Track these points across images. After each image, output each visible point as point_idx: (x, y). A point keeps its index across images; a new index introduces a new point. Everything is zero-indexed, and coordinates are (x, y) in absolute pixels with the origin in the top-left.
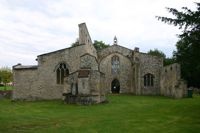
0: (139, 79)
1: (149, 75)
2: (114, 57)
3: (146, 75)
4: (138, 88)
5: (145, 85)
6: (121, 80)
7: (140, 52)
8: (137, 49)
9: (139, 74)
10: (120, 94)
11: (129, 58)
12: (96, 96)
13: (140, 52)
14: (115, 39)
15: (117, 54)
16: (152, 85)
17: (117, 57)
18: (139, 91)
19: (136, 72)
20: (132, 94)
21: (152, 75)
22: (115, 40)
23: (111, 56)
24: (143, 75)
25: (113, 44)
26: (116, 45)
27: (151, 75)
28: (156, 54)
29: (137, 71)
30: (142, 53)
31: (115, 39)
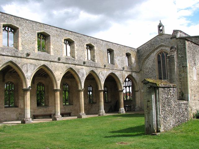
15: (163, 48)
23: (156, 52)
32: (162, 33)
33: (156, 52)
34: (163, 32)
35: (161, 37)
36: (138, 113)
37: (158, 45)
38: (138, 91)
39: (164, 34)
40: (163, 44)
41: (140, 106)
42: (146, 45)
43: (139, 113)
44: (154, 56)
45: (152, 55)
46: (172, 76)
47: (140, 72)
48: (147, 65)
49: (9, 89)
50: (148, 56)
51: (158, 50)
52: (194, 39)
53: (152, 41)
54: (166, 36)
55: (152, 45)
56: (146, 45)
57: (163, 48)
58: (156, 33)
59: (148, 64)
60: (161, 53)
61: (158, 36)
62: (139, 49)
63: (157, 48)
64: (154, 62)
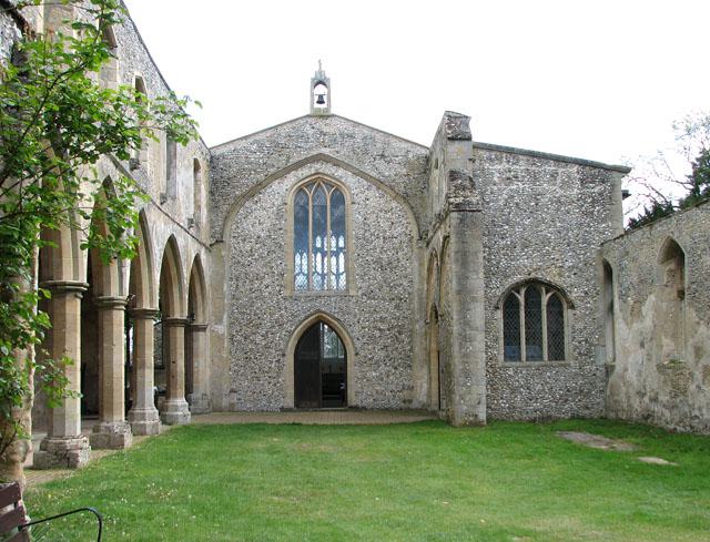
0: (478, 313)
1: (533, 286)
2: (308, 185)
3: (517, 287)
4: (467, 374)
5: (513, 354)
6: (355, 336)
7: (476, 139)
8: (455, 129)
9: (477, 281)
10: (353, 419)
11: (405, 198)
12: (298, 424)
13: (476, 139)
14: (320, 81)
15: (328, 169)
16: (557, 353)
17: (329, 185)
18: (473, 397)
19: (452, 267)
20: (434, 417)
21: (562, 291)
22: (321, 89)
23: (291, 180)
24: (499, 289)
25: (308, 111)
26: (325, 116)
27: (549, 286)
28: (603, 178)
29: (464, 259)
30: (490, 148)
31: (320, 81)
32: (327, 110)
33: (294, 180)
34: (329, 105)
35: (320, 124)
36: (262, 421)
37: (304, 155)
38: (204, 330)
39: (333, 116)
40: (326, 151)
41: (208, 393)
42: (251, 140)
43: (304, 422)
44: (283, 190)
45: (275, 185)
46: (467, 278)
47: (214, 249)
48: (247, 225)
49: (337, 270)
50: (259, 187)
51: (305, 172)
52: (525, 158)
53: (283, 132)
54: (343, 126)
55: (278, 147)
56: (251, 140)
57: (328, 169)
58: (300, 106)
59: (251, 219)
60: (316, 182)
61: (308, 116)
62: (218, 152)
63: (299, 165)
64: (279, 215)
